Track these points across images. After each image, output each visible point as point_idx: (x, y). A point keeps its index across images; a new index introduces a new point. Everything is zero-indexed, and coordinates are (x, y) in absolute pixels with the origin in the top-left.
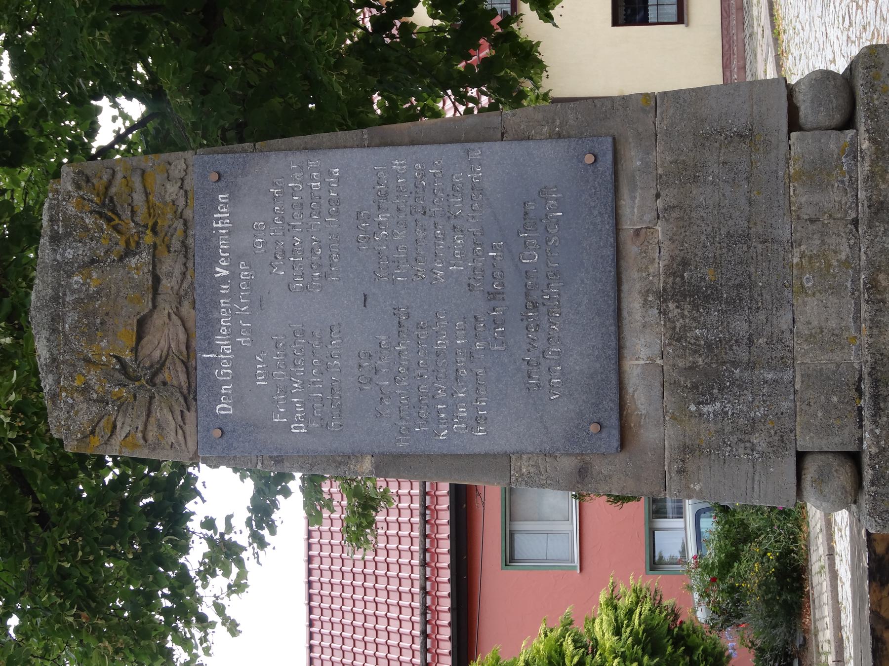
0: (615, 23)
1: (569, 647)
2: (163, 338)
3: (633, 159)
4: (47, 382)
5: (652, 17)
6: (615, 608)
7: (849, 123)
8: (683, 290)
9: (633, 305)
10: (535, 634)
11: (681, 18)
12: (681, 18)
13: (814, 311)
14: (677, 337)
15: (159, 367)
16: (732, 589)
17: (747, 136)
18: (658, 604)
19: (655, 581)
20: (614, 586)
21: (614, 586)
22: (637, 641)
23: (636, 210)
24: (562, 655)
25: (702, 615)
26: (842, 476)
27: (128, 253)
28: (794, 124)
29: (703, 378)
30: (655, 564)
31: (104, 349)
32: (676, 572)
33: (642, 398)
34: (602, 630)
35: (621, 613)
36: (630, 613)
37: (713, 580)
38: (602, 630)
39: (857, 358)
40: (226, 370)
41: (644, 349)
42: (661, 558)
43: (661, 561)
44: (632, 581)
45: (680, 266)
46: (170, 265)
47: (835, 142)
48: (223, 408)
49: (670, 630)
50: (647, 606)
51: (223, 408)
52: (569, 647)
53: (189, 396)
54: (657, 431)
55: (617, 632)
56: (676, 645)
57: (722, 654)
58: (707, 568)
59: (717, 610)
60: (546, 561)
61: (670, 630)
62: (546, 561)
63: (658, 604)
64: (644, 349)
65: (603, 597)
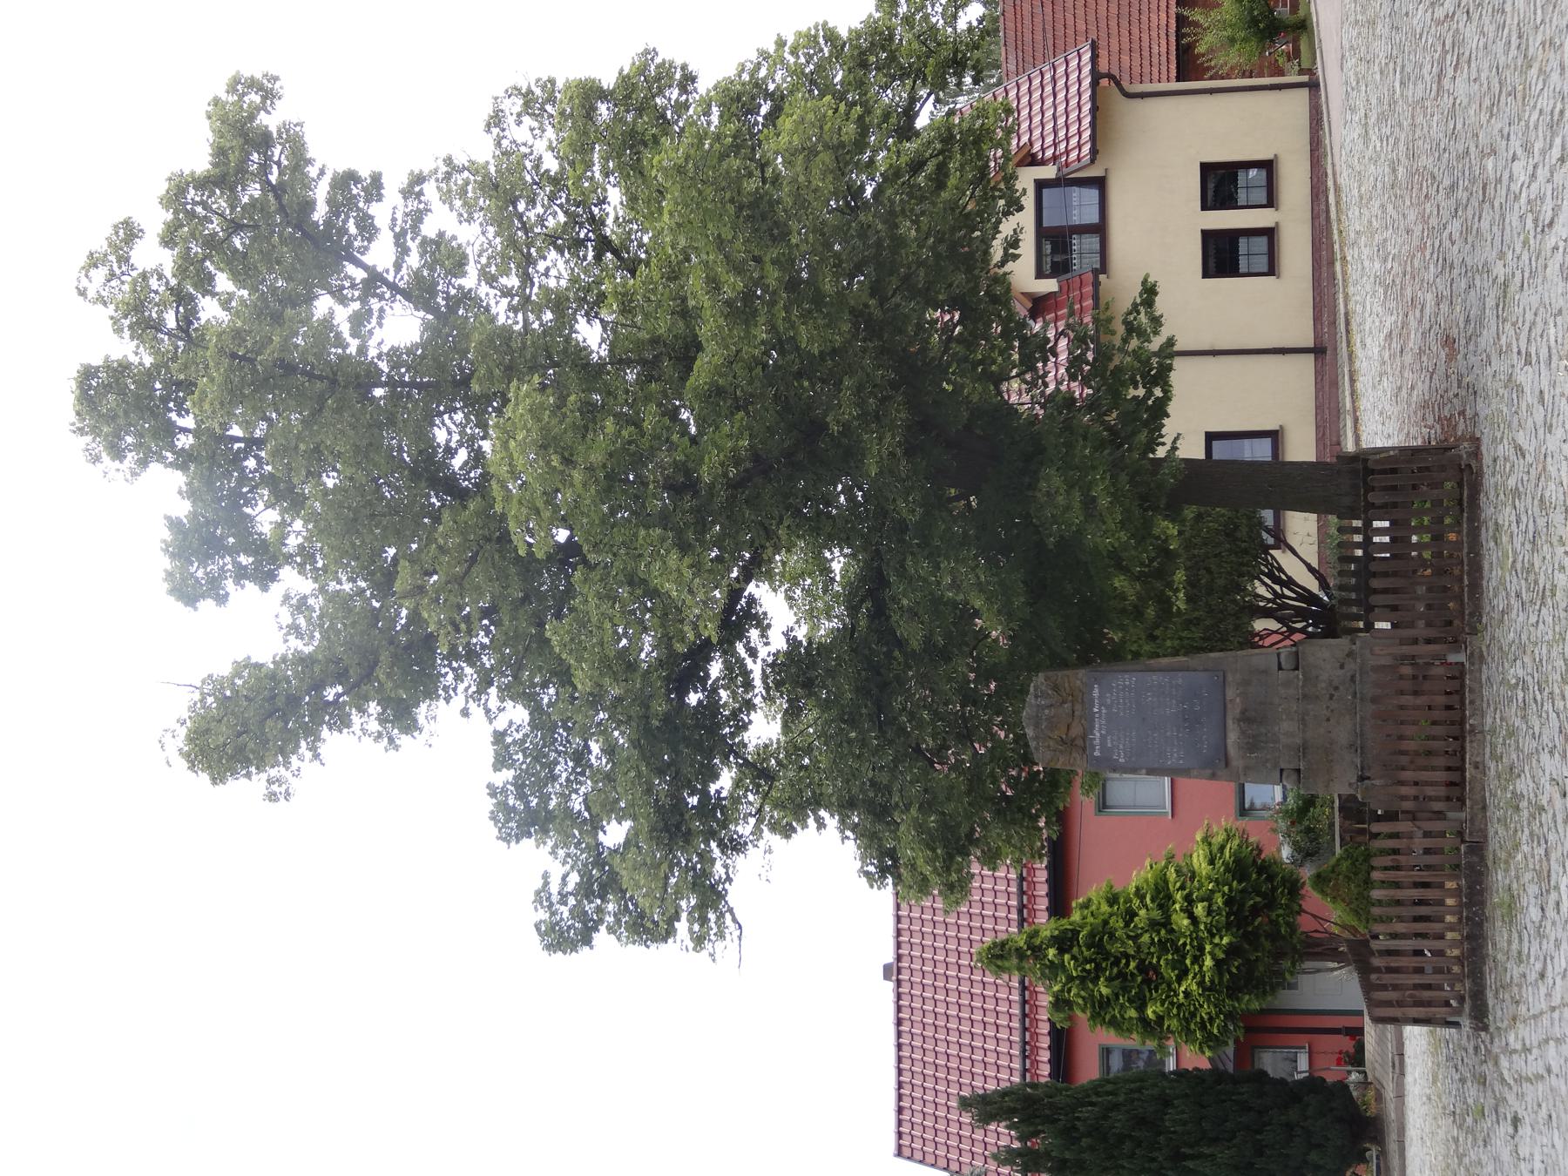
0: (1206, 274)
1: (1172, 875)
2: (1076, 731)
3: (1230, 678)
4: (1033, 744)
5: (1243, 268)
6: (1210, 844)
7: (1297, 668)
8: (1245, 719)
9: (1230, 722)
10: (1142, 866)
11: (1272, 270)
12: (1272, 270)
13: (1286, 726)
14: (1243, 733)
15: (1073, 740)
16: (1309, 830)
17: (1265, 672)
18: (1245, 841)
19: (1243, 823)
20: (1209, 826)
21: (1209, 826)
22: (1228, 870)
23: (1230, 693)
24: (1166, 882)
25: (1286, 852)
26: (1294, 777)
27: (1064, 702)
28: (1280, 668)
29: (1252, 745)
30: (1243, 811)
31: (1055, 735)
32: (1262, 818)
33: (1232, 751)
34: (1199, 862)
35: (1215, 849)
36: (1222, 848)
37: (1293, 823)
38: (1199, 862)
39: (1298, 741)
40: (1097, 741)
41: (1233, 736)
42: (1252, 804)
43: (1252, 808)
44: (1224, 823)
45: (1243, 712)
46: (1078, 707)
47: (1292, 674)
48: (1097, 753)
49: (1254, 861)
50: (1236, 842)
51: (1097, 753)
52: (1172, 875)
53: (1084, 749)
54: (1237, 761)
55: (1212, 862)
56: (1259, 873)
57: (1297, 881)
58: (1287, 813)
59: (1296, 847)
60: (1135, 807)
61: (1254, 861)
62: (1135, 807)
63: (1245, 841)
64: (1233, 736)
65: (1198, 837)
